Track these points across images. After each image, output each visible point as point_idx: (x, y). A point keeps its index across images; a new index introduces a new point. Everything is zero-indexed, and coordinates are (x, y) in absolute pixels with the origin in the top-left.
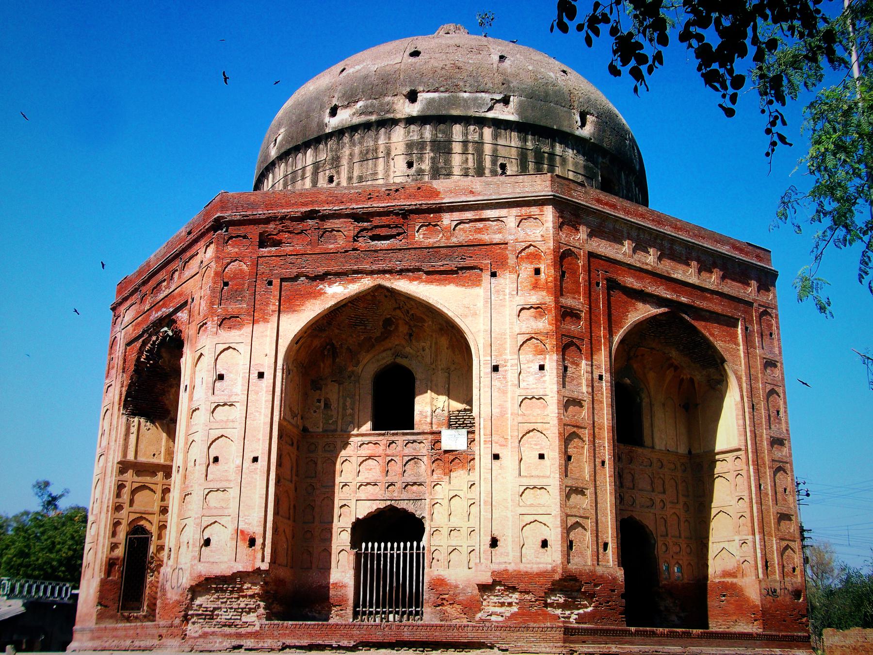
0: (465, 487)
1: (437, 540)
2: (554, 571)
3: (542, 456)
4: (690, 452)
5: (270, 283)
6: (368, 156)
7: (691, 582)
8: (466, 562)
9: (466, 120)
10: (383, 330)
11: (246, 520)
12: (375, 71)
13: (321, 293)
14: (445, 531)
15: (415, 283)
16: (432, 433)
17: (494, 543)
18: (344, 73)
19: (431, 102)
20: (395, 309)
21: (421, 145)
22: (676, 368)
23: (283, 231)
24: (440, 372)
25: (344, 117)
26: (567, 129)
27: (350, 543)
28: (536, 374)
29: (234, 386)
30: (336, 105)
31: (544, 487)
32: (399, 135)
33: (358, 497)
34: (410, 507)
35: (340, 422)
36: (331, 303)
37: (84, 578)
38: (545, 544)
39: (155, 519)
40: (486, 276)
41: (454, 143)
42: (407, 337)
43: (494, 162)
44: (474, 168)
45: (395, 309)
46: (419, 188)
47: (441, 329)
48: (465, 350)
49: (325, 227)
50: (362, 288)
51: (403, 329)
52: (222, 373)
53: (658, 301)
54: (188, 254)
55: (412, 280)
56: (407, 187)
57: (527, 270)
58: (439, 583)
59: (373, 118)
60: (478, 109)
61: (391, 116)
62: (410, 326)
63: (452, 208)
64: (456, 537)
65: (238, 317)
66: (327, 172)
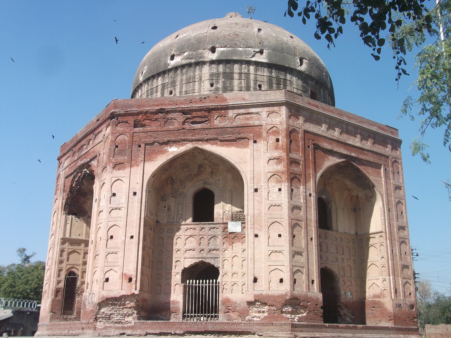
0: (240, 251)
1: (225, 279)
2: (286, 295)
3: (280, 236)
4: (356, 233)
5: (140, 146)
6: (190, 80)
7: (357, 300)
8: (241, 290)
9: (241, 62)
10: (198, 170)
11: (127, 269)
12: (194, 37)
13: (166, 151)
14: (230, 274)
15: (215, 146)
16: (224, 223)
17: (255, 280)
18: (178, 38)
19: (223, 52)
20: (204, 159)
21: (218, 74)
22: (349, 190)
23: (146, 119)
24: (227, 192)
25: (178, 60)
26: (292, 67)
27: (181, 280)
28: (277, 193)
29: (121, 199)
30: (173, 54)
31: (281, 251)
32: (206, 69)
33: (185, 256)
34: (212, 262)
35: (175, 218)
36: (171, 156)
37: (43, 299)
38: (281, 281)
39: (80, 268)
40: (251, 142)
41: (234, 74)
42: (210, 174)
43: (255, 84)
44: (245, 87)
45: (204, 159)
46: (216, 97)
47: (228, 170)
48: (240, 181)
49: (168, 117)
50: (187, 149)
51: (208, 170)
52: (115, 192)
53: (341, 155)
54: (97, 131)
55: (213, 144)
56: (210, 96)
57: (272, 139)
58: (227, 301)
59: (193, 61)
60: (247, 56)
61: (202, 60)
62: (212, 168)
63: (234, 107)
64: (236, 277)
65: (123, 164)
66: (169, 89)
